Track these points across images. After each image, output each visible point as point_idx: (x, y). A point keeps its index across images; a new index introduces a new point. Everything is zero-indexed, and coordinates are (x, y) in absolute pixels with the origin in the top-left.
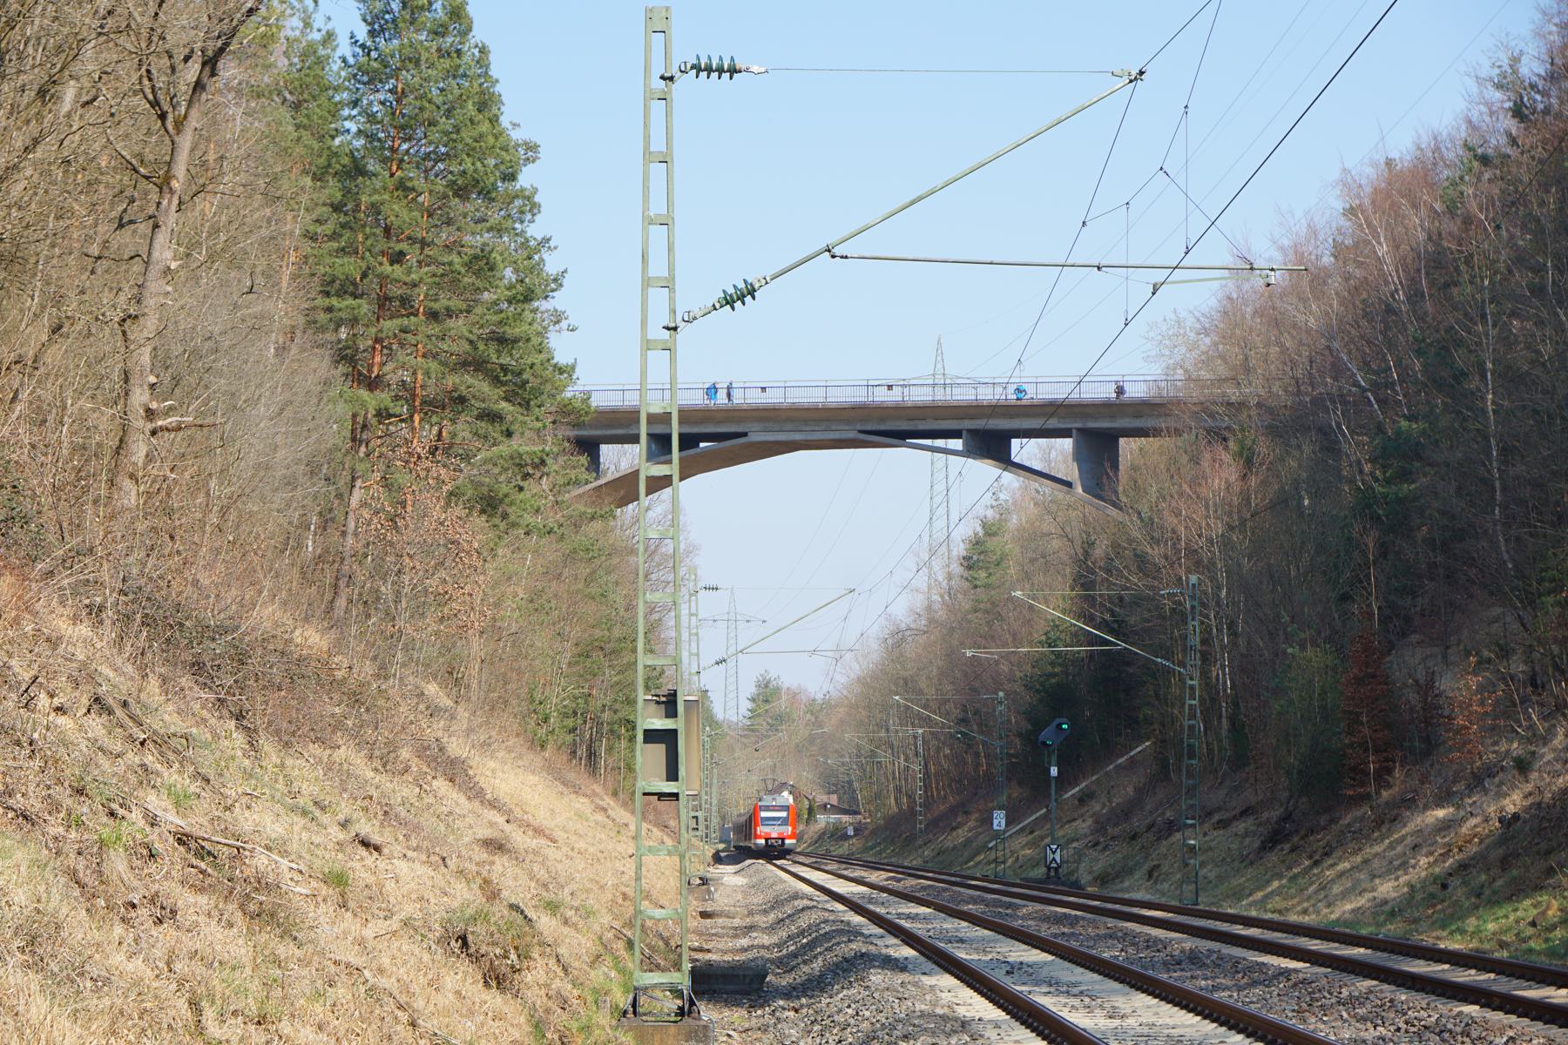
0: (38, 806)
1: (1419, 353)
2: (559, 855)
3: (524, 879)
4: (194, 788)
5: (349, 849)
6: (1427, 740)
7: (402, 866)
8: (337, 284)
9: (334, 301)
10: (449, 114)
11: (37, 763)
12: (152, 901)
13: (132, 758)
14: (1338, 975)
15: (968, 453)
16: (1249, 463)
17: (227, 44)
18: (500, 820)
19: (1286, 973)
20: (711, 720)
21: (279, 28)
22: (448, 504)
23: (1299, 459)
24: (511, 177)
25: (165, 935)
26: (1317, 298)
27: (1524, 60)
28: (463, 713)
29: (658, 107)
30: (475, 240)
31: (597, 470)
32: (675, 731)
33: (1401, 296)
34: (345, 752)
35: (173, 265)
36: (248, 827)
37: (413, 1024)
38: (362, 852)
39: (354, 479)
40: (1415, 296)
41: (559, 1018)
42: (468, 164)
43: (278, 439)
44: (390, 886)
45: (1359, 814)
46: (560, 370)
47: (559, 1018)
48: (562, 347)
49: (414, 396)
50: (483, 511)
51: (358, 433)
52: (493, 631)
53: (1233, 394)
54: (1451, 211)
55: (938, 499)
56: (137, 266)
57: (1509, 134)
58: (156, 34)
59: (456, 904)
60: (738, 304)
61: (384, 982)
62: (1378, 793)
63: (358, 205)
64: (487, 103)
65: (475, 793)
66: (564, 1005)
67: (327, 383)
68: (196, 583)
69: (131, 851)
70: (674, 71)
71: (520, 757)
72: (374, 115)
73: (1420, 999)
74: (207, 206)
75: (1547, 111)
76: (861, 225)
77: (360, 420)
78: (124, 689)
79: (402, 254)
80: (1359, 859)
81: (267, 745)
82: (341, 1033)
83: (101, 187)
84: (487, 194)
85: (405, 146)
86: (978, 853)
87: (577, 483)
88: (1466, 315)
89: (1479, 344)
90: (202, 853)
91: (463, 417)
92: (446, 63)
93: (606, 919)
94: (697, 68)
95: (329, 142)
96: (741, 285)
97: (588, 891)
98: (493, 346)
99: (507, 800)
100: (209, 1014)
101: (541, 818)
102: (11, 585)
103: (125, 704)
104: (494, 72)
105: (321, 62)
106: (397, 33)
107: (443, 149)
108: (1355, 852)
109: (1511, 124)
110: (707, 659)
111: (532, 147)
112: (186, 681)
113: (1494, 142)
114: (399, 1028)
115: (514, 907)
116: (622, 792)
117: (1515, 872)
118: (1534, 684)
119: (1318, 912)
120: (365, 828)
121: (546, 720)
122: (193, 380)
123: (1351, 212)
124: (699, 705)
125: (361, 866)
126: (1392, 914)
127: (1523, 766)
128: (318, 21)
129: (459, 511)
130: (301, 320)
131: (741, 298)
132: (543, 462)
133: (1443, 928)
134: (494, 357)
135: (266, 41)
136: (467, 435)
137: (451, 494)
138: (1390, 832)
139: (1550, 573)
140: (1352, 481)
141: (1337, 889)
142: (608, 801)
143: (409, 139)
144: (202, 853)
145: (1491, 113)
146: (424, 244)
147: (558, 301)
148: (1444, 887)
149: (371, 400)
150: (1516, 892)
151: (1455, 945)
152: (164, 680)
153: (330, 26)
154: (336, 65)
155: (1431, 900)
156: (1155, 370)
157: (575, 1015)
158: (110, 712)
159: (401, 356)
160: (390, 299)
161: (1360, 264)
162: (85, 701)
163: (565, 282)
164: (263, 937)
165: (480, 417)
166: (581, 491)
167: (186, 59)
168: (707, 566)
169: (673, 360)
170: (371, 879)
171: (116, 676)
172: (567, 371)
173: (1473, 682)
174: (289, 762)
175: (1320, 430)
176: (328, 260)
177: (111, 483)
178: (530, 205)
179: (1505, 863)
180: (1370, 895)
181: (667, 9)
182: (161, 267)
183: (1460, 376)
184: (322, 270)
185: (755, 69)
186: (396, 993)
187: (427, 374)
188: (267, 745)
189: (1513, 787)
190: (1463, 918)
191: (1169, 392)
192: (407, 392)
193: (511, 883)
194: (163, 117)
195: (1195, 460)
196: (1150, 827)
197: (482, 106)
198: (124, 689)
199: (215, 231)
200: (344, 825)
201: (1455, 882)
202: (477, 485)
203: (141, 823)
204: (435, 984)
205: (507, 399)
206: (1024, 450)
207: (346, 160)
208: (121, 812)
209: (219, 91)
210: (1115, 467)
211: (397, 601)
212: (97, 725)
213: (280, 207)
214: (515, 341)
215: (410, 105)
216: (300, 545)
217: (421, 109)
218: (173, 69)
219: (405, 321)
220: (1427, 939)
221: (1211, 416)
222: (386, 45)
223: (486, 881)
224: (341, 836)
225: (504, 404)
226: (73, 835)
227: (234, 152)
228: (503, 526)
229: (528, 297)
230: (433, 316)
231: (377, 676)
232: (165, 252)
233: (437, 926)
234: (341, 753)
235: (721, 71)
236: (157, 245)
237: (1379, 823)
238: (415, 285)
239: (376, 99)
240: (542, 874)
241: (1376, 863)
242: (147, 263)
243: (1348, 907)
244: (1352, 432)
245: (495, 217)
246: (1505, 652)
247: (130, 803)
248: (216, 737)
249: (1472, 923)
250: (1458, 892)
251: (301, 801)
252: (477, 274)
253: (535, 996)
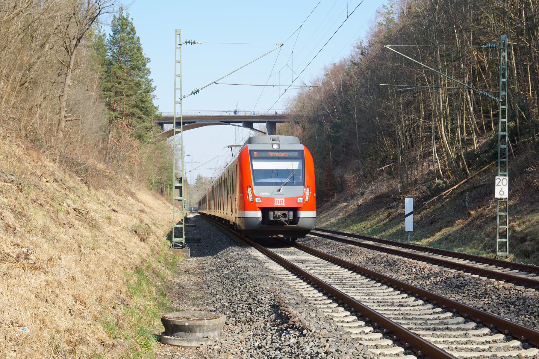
0: (44, 203)
1: (341, 105)
2: (155, 213)
3: (148, 218)
4: (77, 198)
5: (111, 212)
6: (342, 188)
7: (122, 216)
8: (106, 89)
9: (105, 93)
10: (131, 52)
11: (43, 193)
12: (69, 223)
13: (63, 192)
14: (323, 239)
15: (244, 126)
16: (304, 129)
17: (82, 36)
18: (142, 205)
19: (313, 238)
20: (188, 184)
21: (93, 32)
22: (131, 137)
23: (315, 128)
24: (145, 66)
25: (72, 231)
26: (319, 93)
27: (363, 42)
28: (134, 182)
29: (178, 51)
30: (136, 79)
31: (163, 129)
32: (181, 187)
33: (337, 93)
34: (109, 191)
35: (71, 84)
36: (89, 207)
37: (126, 250)
38: (113, 212)
39: (110, 131)
40: (340, 93)
41: (156, 248)
42: (135, 63)
43: (93, 123)
44: (120, 220)
45: (327, 204)
46: (155, 108)
47: (156, 248)
48: (155, 103)
49: (123, 113)
50: (138, 139)
51: (111, 121)
52: (140, 164)
53: (301, 114)
54: (348, 75)
55: (237, 136)
56: (62, 85)
57: (360, 58)
58: (67, 34)
59: (134, 224)
60: (195, 94)
61: (120, 241)
62: (331, 200)
63: (111, 71)
64: (139, 49)
65: (137, 200)
66: (158, 245)
67: (104, 110)
68: (76, 154)
69: (64, 212)
70: (182, 43)
71: (146, 192)
72: (114, 52)
73: (341, 244)
74: (78, 71)
75: (368, 54)
76: (222, 77)
77: (111, 118)
78: (61, 177)
79: (120, 82)
80: (327, 214)
81: (92, 189)
82: (110, 251)
83: (54, 67)
84: (139, 69)
85: (121, 59)
87: (159, 132)
88: (351, 97)
89: (353, 103)
90: (80, 213)
91: (134, 118)
92: (130, 41)
93: (166, 227)
94: (187, 42)
95: (104, 57)
96: (196, 90)
97: (162, 221)
98: (141, 102)
99: (144, 201)
100: (82, 247)
101: (151, 205)
102: (36, 154)
103: (61, 180)
104: (141, 43)
105: (103, 40)
106: (119, 34)
107: (130, 59)
108: (326, 213)
109: (361, 56)
110: (187, 171)
111: (149, 59)
112: (74, 175)
113: (357, 60)
114: (123, 250)
115: (147, 224)
116: (170, 201)
117: (360, 217)
118: (365, 176)
119: (318, 225)
120: (114, 207)
121: (152, 184)
122: (75, 109)
123: (326, 75)
124: (186, 181)
125: (113, 215)
126: (334, 225)
127: (362, 194)
128: (102, 31)
129: (133, 138)
130: (98, 96)
131: (196, 92)
132: (151, 128)
133: (345, 228)
134: (141, 105)
135: (91, 35)
136: (135, 122)
137: (131, 135)
138: (334, 208)
139: (368, 153)
140: (326, 133)
141: (323, 220)
142: (166, 202)
143: (122, 57)
144: (80, 213)
145: (356, 54)
146: (125, 80)
147: (155, 93)
148: (346, 220)
149: (114, 114)
150: (361, 221)
151: (348, 232)
152: (70, 175)
153: (104, 32)
154: (106, 41)
155: (343, 222)
156: (284, 109)
157: (160, 248)
158: (58, 182)
159: (120, 104)
160: (118, 92)
161: (328, 86)
162: (53, 180)
163: (156, 89)
164: (93, 231)
165: (138, 118)
166: (159, 134)
167: (73, 39)
168: (187, 151)
169: (181, 106)
170: (116, 218)
171: (59, 174)
172: (156, 108)
173: (352, 176)
174: (97, 193)
175: (319, 122)
176: (104, 83)
177: (57, 132)
178: (149, 72)
179: (358, 215)
180: (329, 222)
181: (180, 29)
182: (68, 85)
183: (349, 110)
184: (103, 86)
185: (199, 43)
186: (122, 243)
187: (126, 108)
188: (92, 189)
189: (360, 199)
190: (349, 226)
191: (287, 113)
192: (122, 113)
193: (145, 219)
194: (68, 52)
195: (293, 128)
197: (138, 50)
198: (61, 177)
199: (79, 77)
200: (109, 207)
201: (348, 219)
202: (137, 133)
203: (66, 206)
204: (130, 241)
205: (144, 114)
206: (255, 126)
207: (108, 62)
208: (62, 204)
209: (80, 46)
210: (275, 129)
211: (120, 158)
212: (55, 185)
213: (94, 72)
214: (145, 101)
215: (122, 50)
216: (98, 146)
217: (125, 51)
218: (70, 41)
219: (121, 97)
220: (342, 231)
221: (296, 118)
222: (118, 36)
223: (140, 219)
224: (109, 209)
225: (143, 115)
226: (51, 209)
227: (83, 60)
228: (143, 142)
229: (148, 92)
230: (127, 96)
231: (116, 174)
232: (69, 81)
233: (130, 228)
234: (108, 191)
235: (192, 43)
236: (67, 80)
237: (332, 206)
238: (123, 89)
239: (115, 48)
240: (152, 217)
241: (331, 215)
242: (65, 84)
243: (325, 224)
244: (326, 122)
245: (141, 74)
246: (359, 170)
247: (64, 202)
248: (81, 187)
249: (351, 227)
250: (349, 221)
251: (100, 201)
252: (137, 87)
253: (151, 243)
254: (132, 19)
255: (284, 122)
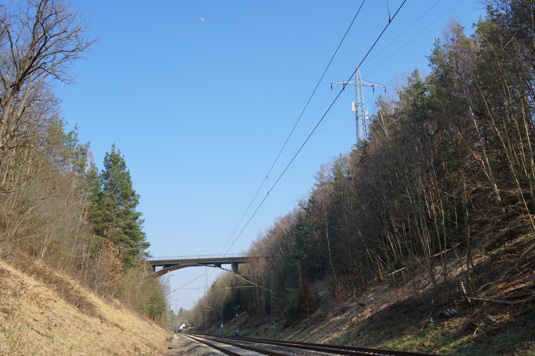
86: (216, 332)
104: (130, 176)
111: (139, 196)
163: (145, 221)
196: (252, 326)
254: (123, 156)
255: (245, 262)
